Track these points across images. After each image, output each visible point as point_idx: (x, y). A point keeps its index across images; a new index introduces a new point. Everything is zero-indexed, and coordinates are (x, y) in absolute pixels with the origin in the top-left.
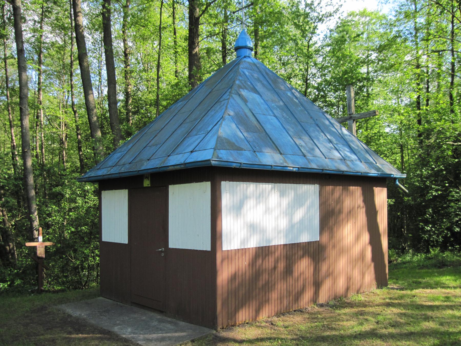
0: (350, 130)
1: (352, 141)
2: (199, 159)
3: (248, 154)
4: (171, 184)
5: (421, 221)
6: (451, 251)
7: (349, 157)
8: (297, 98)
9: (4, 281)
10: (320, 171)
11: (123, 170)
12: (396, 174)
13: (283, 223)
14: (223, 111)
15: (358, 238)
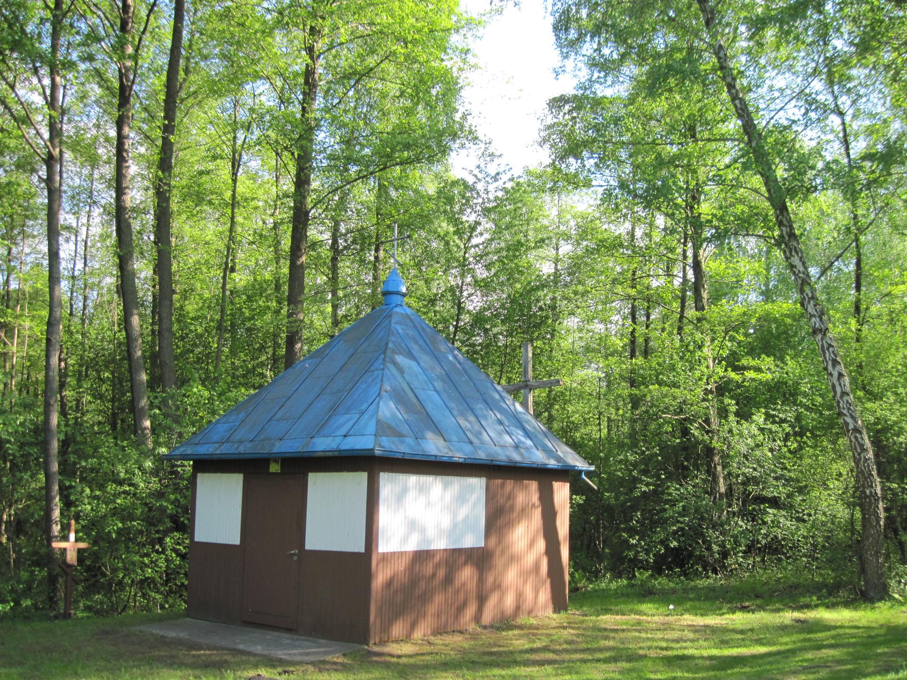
0: (524, 404)
1: (527, 422)
2: (358, 447)
3: (410, 441)
5: (624, 530)
6: (667, 576)
7: (523, 443)
8: (460, 363)
9: (3, 601)
10: (489, 462)
11: (242, 449)
12: (580, 464)
13: (446, 522)
14: (378, 385)
15: (532, 544)
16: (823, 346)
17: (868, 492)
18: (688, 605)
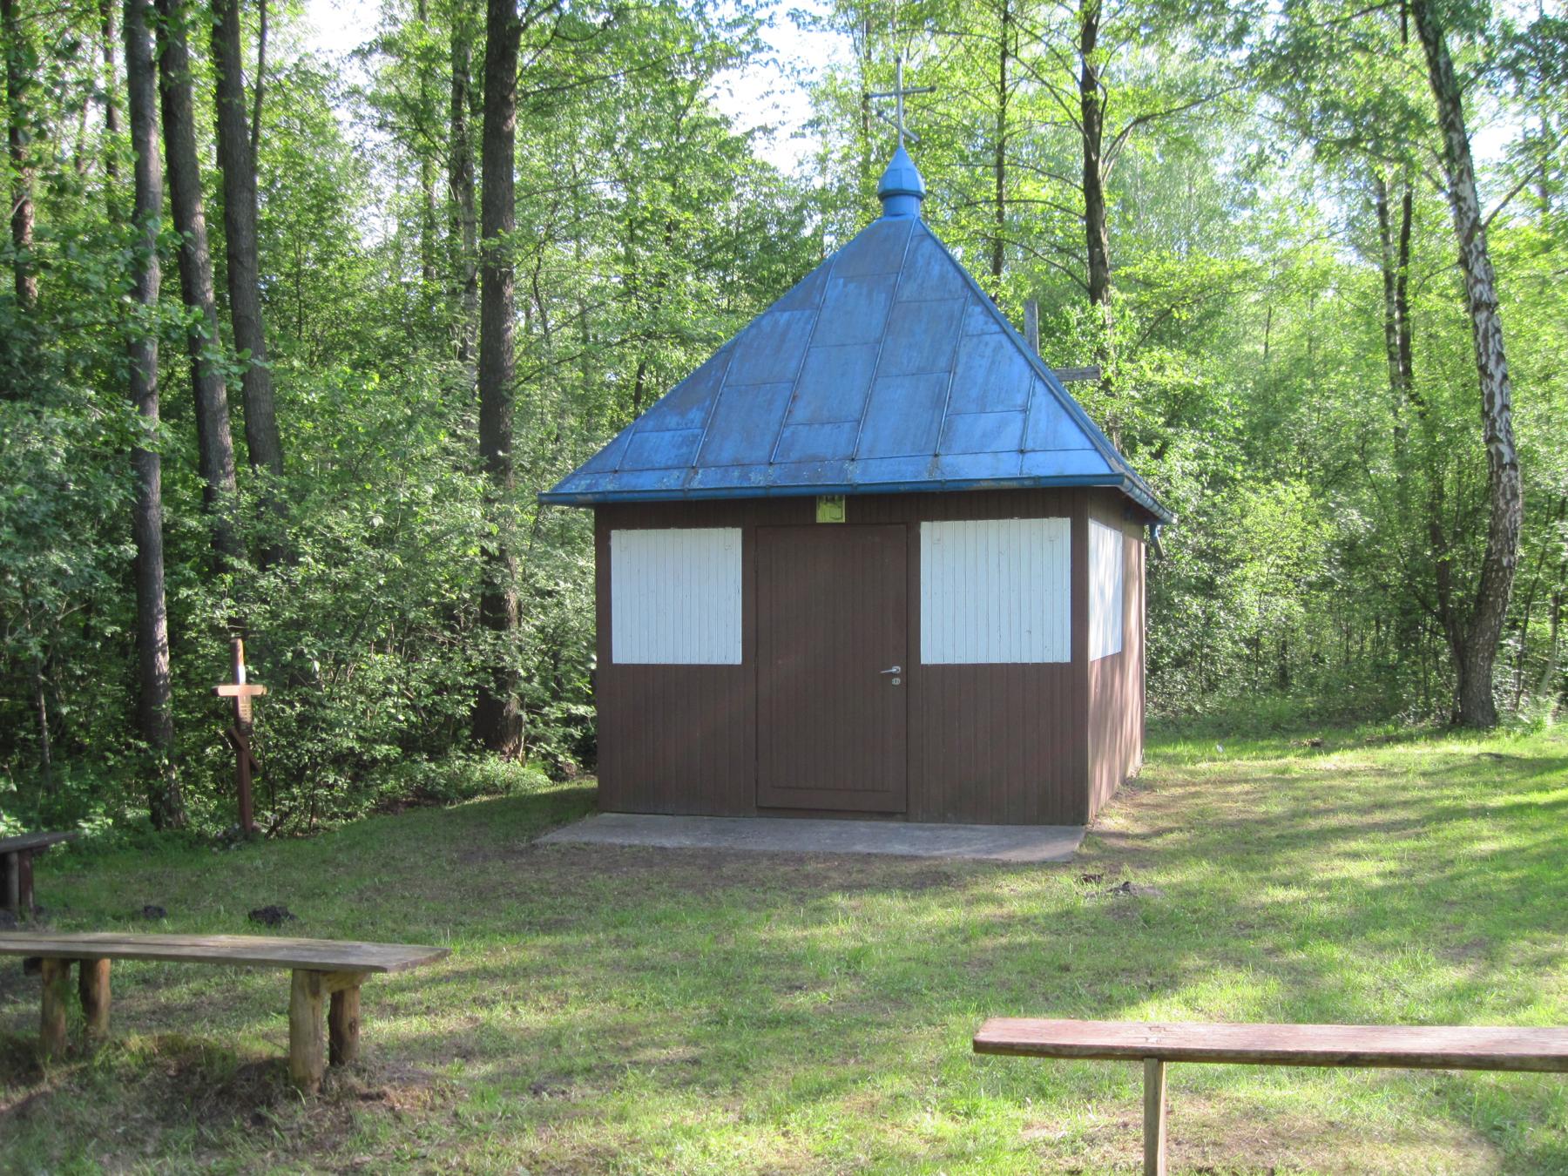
16: (1486, 330)
17: (1505, 562)
18: (1232, 740)
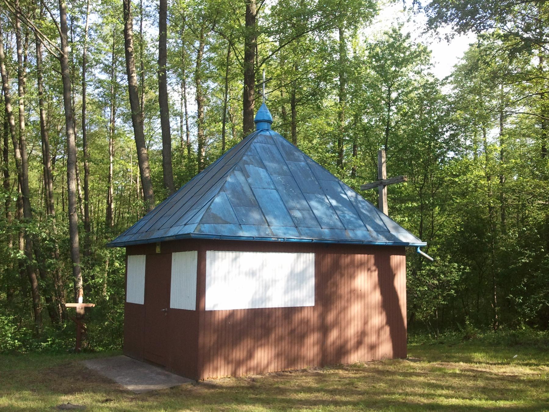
4: (176, 251)
11: (140, 238)
